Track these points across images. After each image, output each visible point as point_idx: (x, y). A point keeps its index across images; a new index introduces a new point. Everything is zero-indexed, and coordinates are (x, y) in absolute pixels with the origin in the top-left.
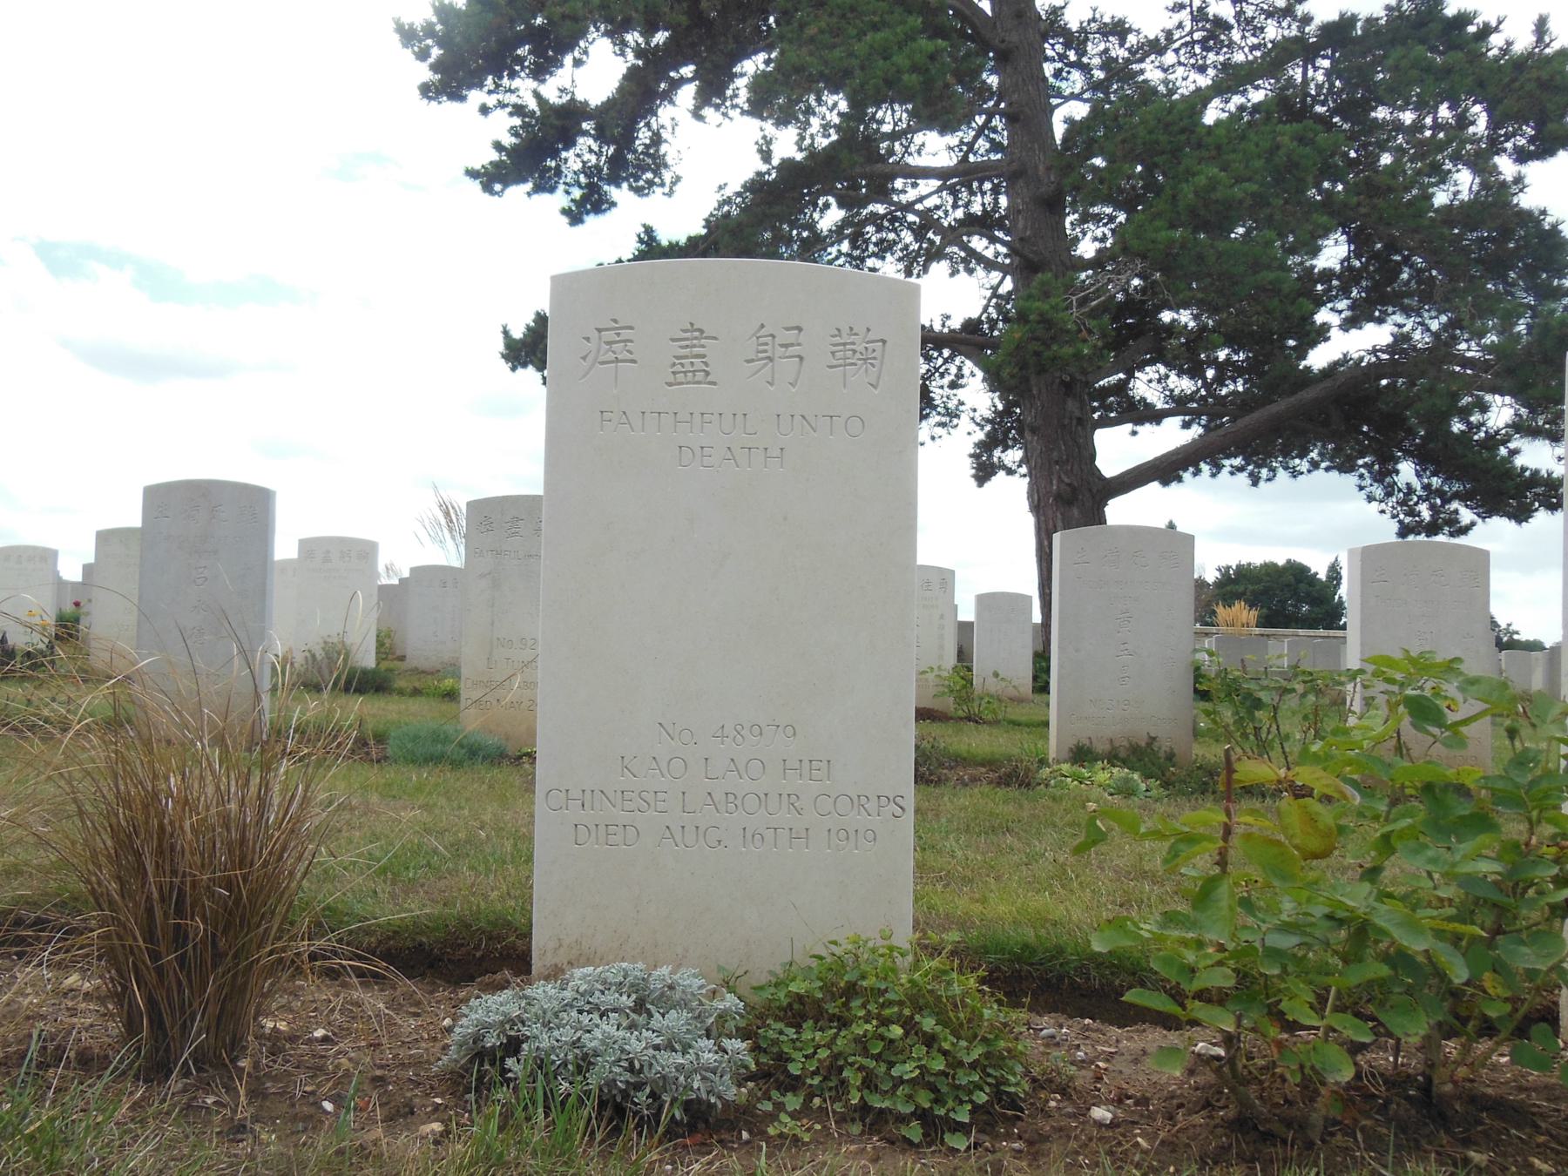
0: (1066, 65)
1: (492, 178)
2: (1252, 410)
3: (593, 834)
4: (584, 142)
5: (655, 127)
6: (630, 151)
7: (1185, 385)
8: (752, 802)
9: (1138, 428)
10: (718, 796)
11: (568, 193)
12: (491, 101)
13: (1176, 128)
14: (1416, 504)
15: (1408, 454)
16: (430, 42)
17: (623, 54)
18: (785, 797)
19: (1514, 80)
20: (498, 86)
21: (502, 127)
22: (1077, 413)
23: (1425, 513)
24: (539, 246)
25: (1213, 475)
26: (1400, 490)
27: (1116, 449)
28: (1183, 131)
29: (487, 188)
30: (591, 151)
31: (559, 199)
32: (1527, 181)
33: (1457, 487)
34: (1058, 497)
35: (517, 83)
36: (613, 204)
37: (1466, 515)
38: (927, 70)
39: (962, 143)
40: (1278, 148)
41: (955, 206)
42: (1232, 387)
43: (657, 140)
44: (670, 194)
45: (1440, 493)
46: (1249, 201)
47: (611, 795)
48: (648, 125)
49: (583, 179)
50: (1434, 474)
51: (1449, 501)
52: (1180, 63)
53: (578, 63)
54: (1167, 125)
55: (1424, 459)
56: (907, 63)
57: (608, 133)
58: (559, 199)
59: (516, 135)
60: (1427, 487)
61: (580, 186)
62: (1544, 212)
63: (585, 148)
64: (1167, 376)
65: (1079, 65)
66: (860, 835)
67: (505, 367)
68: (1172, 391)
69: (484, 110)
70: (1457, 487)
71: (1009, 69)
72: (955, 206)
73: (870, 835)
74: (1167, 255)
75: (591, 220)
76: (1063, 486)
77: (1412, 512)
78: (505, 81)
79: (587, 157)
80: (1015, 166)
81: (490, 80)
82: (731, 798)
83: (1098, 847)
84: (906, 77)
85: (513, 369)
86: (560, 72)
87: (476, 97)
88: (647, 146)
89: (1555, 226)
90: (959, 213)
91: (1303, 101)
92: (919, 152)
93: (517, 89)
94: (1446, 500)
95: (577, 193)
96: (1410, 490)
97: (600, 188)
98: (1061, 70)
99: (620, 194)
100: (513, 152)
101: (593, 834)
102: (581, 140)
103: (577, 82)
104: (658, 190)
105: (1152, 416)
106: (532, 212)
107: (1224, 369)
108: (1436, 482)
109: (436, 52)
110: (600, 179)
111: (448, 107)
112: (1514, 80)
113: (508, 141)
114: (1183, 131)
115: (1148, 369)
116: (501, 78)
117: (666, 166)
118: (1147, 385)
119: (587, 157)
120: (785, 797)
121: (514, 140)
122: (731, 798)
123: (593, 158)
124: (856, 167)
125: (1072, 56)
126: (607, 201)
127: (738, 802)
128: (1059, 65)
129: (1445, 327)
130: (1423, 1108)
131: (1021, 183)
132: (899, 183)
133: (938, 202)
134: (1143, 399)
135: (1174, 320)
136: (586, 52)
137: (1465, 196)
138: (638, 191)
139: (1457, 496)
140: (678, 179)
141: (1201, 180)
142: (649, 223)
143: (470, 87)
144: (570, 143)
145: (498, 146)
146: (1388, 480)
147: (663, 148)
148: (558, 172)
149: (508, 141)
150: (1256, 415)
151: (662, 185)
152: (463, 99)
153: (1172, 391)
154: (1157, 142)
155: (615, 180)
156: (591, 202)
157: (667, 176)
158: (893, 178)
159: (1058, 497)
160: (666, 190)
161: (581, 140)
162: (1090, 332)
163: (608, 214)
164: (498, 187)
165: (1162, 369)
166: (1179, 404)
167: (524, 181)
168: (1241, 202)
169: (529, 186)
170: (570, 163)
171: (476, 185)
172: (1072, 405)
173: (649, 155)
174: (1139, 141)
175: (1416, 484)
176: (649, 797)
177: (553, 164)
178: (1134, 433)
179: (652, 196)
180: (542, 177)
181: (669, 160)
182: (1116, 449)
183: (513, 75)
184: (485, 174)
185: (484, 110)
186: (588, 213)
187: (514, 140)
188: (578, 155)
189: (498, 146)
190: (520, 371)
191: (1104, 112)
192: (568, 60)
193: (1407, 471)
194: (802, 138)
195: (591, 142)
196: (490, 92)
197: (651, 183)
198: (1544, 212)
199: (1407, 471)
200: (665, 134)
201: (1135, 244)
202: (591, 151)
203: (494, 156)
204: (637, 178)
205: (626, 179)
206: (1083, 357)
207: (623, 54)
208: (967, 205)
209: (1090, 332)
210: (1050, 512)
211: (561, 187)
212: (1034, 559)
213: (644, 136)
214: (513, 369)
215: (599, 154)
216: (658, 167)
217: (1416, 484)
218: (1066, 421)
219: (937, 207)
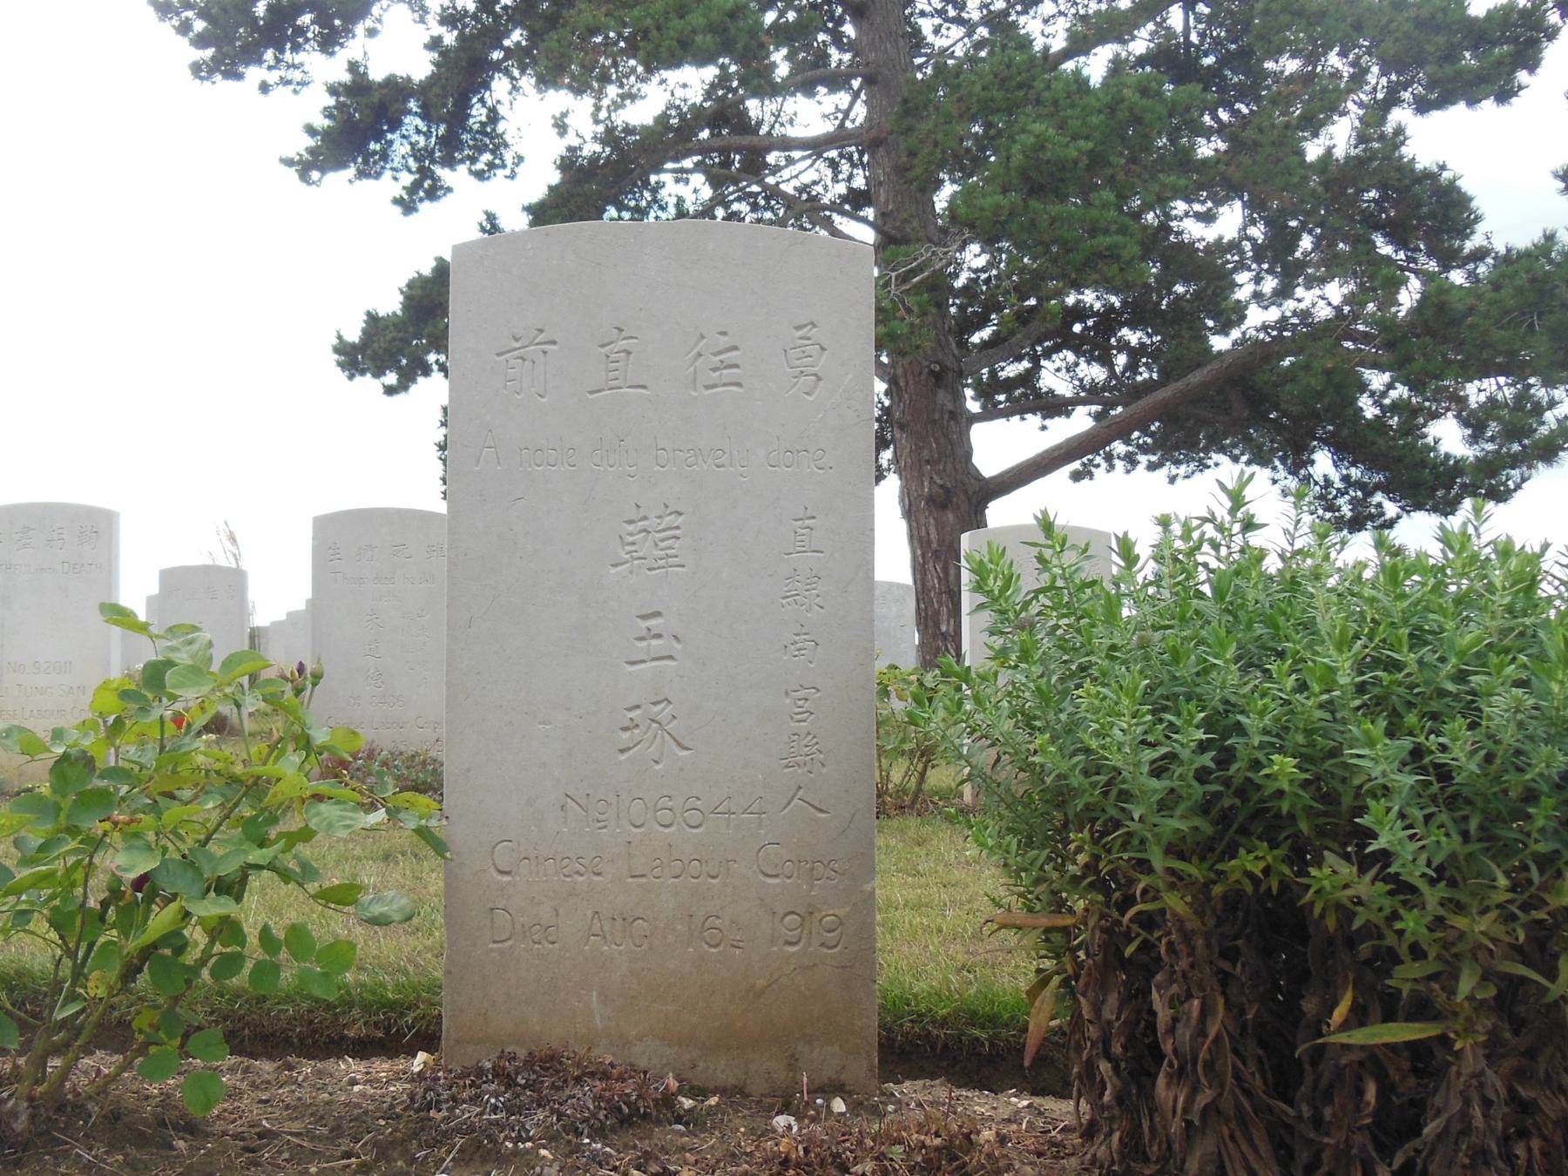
0: (946, 20)
1: (308, 167)
2: (1138, 398)
4: (412, 122)
5: (489, 103)
6: (464, 129)
7: (1097, 373)
9: (1048, 422)
11: (396, 179)
12: (272, 77)
13: (1013, 83)
14: (1335, 497)
15: (1325, 442)
16: (190, 14)
17: (422, 21)
19: (1391, 21)
20: (278, 61)
21: (314, 106)
22: (950, 406)
23: (1346, 511)
24: (375, 241)
25: (1128, 472)
26: (1316, 483)
27: (997, 444)
28: (1020, 86)
29: (304, 176)
30: (418, 132)
31: (392, 185)
32: (1408, 133)
33: (1378, 478)
34: (930, 500)
35: (299, 58)
36: (449, 190)
37: (1391, 509)
38: (725, 30)
39: (838, 110)
40: (1123, 100)
41: (835, 180)
42: (1146, 375)
43: (494, 117)
44: (512, 176)
45: (1359, 485)
46: (1085, 161)
48: (482, 100)
49: (412, 163)
50: (1354, 464)
51: (1371, 494)
52: (1061, 13)
53: (372, 33)
54: (1004, 80)
55: (1343, 450)
56: (702, 21)
57: (433, 112)
58: (392, 185)
59: (330, 116)
60: (1346, 479)
61: (410, 171)
62: (1443, 168)
63: (411, 128)
64: (1077, 364)
65: (959, 21)
67: (341, 376)
68: (1081, 380)
69: (264, 88)
70: (1378, 478)
71: (865, 26)
72: (835, 180)
74: (996, 222)
75: (426, 207)
76: (936, 489)
77: (1331, 507)
78: (288, 56)
79: (415, 138)
80: (873, 133)
81: (269, 55)
84: (699, 38)
85: (351, 377)
86: (350, 43)
87: (254, 74)
88: (483, 124)
89: (1452, 182)
90: (841, 188)
91: (1187, 50)
92: (791, 122)
93: (302, 64)
94: (1368, 491)
95: (407, 179)
96: (1328, 483)
97: (433, 172)
98: (940, 26)
99: (456, 177)
100: (326, 134)
102: (407, 120)
103: (370, 54)
104: (500, 172)
105: (1055, 407)
106: (360, 199)
107: (1135, 353)
108: (1355, 473)
109: (199, 26)
110: (433, 162)
111: (221, 84)
112: (1391, 21)
113: (321, 122)
114: (1020, 86)
115: (1054, 357)
116: (282, 51)
117: (506, 145)
118: (1054, 378)
119: (415, 138)
121: (327, 123)
123: (422, 141)
124: (727, 142)
125: (952, 13)
126: (442, 187)
128: (937, 21)
129: (1347, 299)
131: (881, 151)
132: (771, 158)
133: (816, 177)
134: (1051, 391)
135: (1079, 301)
136: (379, 21)
137: (1339, 153)
138: (480, 175)
139: (1378, 487)
140: (520, 159)
141: (1029, 140)
142: (492, 209)
143: (247, 64)
144: (395, 125)
145: (311, 130)
146: (1302, 472)
147: (501, 127)
148: (385, 156)
149: (321, 122)
150: (1141, 403)
151: (504, 166)
152: (239, 77)
153: (1081, 380)
154: (992, 100)
155: (450, 162)
156: (425, 189)
157: (508, 156)
158: (768, 150)
159: (930, 500)
160: (508, 172)
161: (407, 120)
162: (909, 311)
163: (443, 200)
164: (315, 175)
165: (1070, 356)
166: (1091, 393)
167: (344, 166)
168: (1075, 162)
169: (351, 171)
170: (396, 146)
171: (292, 173)
172: (942, 397)
173: (486, 134)
174: (974, 99)
175: (1335, 476)
177: (378, 147)
178: (1044, 428)
179: (494, 181)
180: (366, 162)
181: (507, 137)
182: (997, 444)
183: (296, 48)
184: (300, 162)
185: (264, 88)
186: (421, 200)
187: (327, 123)
188: (404, 137)
189: (311, 130)
190: (358, 379)
192: (360, 29)
193: (1323, 463)
194: (598, 108)
195: (418, 121)
196: (270, 68)
197: (491, 166)
198: (1443, 168)
199: (1323, 463)
200: (502, 110)
201: (962, 211)
202: (418, 132)
203: (310, 142)
204: (473, 160)
205: (462, 161)
206: (899, 337)
207: (422, 21)
208: (850, 177)
209: (909, 311)
210: (922, 520)
211: (388, 174)
213: (478, 113)
214: (351, 377)
215: (428, 135)
216: (497, 147)
217: (1335, 476)
218: (937, 416)
219: (815, 183)
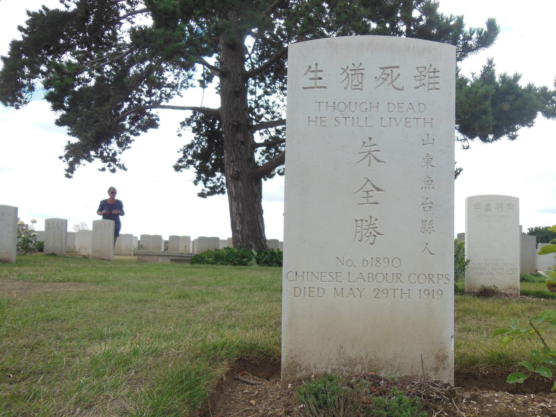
3: (303, 292)
8: (380, 277)
10: (365, 275)
18: (395, 275)
22: (242, 139)
47: (316, 274)
66: (435, 292)
73: (440, 292)
82: (371, 275)
83: (22, 269)
101: (303, 292)
120: (395, 275)
121: (28, 26)
122: (371, 275)
127: (374, 277)
130: (475, 374)
176: (334, 275)
189: (20, 29)
191: (214, 50)
212: (263, 187)
214: (211, 82)
